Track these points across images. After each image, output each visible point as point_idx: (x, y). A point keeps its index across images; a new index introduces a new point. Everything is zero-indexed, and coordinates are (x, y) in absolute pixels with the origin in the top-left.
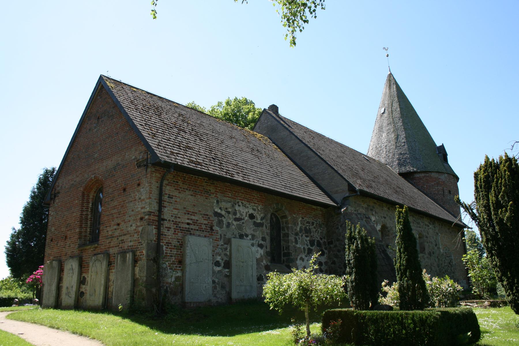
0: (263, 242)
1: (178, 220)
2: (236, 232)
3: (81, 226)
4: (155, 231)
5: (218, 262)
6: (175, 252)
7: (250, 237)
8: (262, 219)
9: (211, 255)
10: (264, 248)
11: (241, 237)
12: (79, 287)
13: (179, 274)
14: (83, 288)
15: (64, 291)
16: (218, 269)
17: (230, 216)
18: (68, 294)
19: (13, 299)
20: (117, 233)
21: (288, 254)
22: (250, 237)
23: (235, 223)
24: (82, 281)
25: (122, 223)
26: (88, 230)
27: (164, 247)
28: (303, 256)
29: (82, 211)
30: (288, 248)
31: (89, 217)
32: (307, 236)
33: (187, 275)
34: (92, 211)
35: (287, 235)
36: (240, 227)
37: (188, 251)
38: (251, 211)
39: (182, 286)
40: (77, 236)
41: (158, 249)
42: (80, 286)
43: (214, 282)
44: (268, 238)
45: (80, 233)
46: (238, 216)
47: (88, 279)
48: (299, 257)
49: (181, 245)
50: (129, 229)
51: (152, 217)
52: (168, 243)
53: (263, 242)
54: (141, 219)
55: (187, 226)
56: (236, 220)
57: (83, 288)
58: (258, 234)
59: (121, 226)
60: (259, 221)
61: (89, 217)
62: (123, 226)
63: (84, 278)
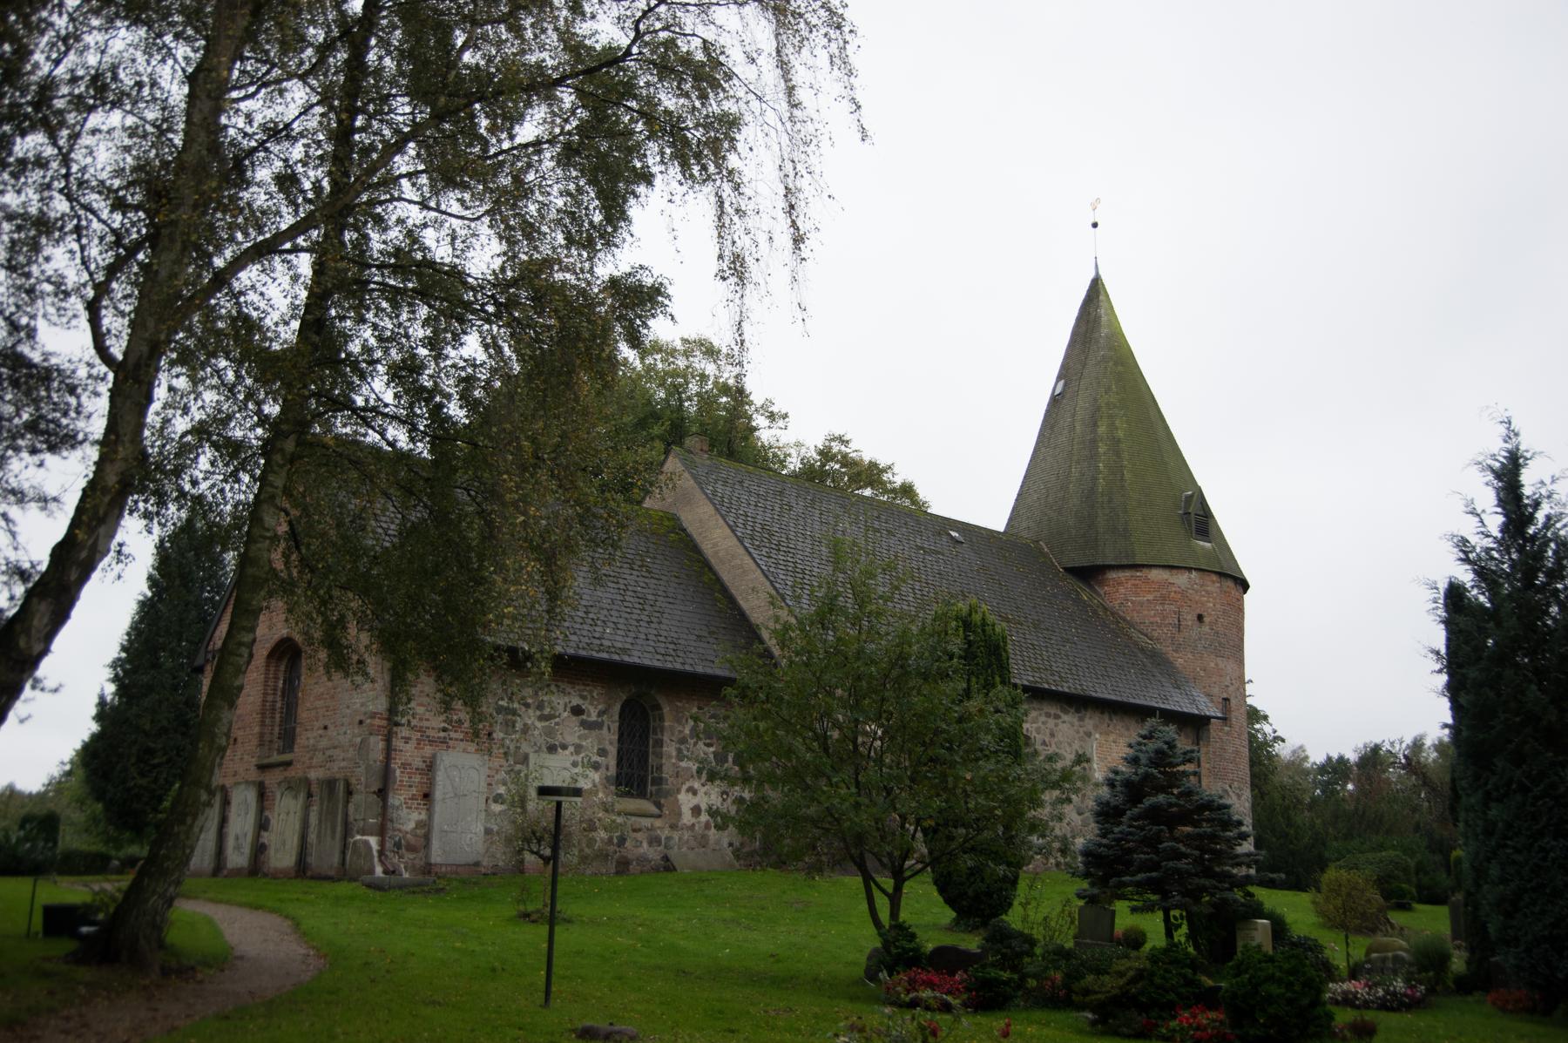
0: (599, 759)
1: (426, 724)
2: (541, 741)
3: (263, 724)
4: (381, 745)
5: (500, 795)
6: (417, 779)
7: (571, 749)
8: (600, 714)
9: (484, 784)
10: (603, 770)
11: (552, 749)
12: (257, 836)
13: (423, 816)
14: (266, 837)
15: (230, 843)
16: (497, 808)
17: (531, 711)
18: (238, 848)
19: (734, 680)
20: (324, 743)
21: (658, 781)
22: (571, 749)
23: (539, 725)
24: (262, 825)
25: (331, 728)
26: (277, 729)
27: (398, 773)
28: (696, 785)
29: (265, 694)
30: (659, 768)
31: (279, 705)
32: (709, 745)
33: (437, 819)
34: (283, 696)
35: (659, 743)
36: (549, 732)
37: (440, 777)
38: (576, 701)
39: (427, 838)
40: (255, 742)
41: (386, 774)
42: (312, 878)
43: (488, 832)
44: (613, 751)
45: (262, 735)
46: (547, 711)
47: (273, 822)
48: (685, 787)
49: (430, 767)
50: (341, 738)
51: (377, 722)
52: (404, 766)
53: (599, 759)
54: (361, 722)
55: (442, 734)
56: (542, 718)
57: (266, 837)
58: (590, 743)
59: (329, 732)
60: (594, 718)
61: (279, 705)
62: (332, 732)
63: (268, 820)
